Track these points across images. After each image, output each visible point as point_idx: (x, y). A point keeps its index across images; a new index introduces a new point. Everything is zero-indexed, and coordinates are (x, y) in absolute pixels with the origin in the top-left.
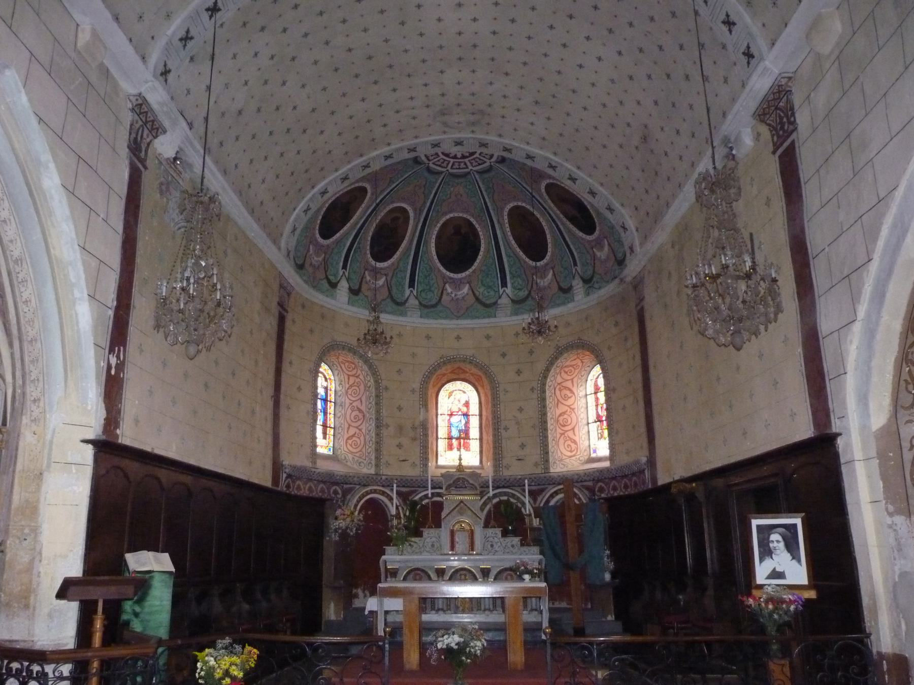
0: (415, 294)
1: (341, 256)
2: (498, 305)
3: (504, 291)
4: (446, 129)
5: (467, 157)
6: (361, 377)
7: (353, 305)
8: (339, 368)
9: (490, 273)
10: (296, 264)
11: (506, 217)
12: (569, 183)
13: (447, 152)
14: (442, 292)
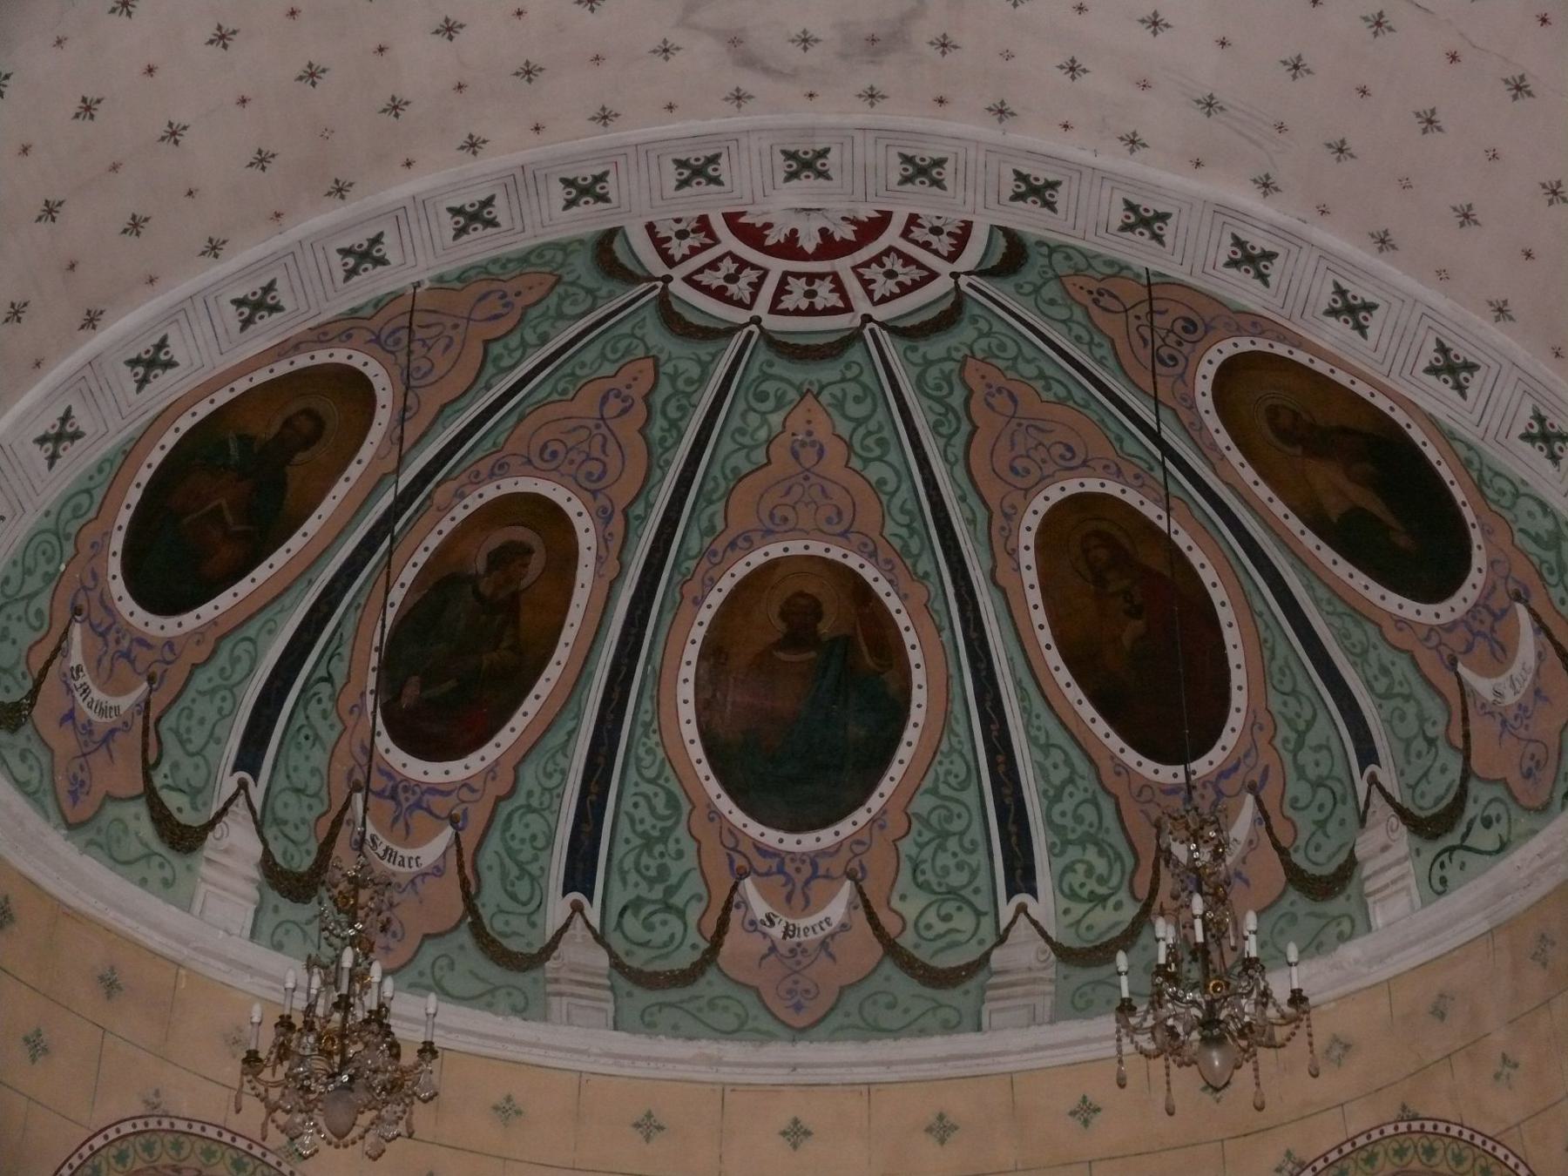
0: (595, 922)
1: (236, 705)
2: (992, 974)
3: (1022, 909)
4: (748, 81)
5: (846, 248)
7: (278, 947)
9: (957, 826)
11: (1028, 558)
12: (1334, 334)
13: (753, 218)
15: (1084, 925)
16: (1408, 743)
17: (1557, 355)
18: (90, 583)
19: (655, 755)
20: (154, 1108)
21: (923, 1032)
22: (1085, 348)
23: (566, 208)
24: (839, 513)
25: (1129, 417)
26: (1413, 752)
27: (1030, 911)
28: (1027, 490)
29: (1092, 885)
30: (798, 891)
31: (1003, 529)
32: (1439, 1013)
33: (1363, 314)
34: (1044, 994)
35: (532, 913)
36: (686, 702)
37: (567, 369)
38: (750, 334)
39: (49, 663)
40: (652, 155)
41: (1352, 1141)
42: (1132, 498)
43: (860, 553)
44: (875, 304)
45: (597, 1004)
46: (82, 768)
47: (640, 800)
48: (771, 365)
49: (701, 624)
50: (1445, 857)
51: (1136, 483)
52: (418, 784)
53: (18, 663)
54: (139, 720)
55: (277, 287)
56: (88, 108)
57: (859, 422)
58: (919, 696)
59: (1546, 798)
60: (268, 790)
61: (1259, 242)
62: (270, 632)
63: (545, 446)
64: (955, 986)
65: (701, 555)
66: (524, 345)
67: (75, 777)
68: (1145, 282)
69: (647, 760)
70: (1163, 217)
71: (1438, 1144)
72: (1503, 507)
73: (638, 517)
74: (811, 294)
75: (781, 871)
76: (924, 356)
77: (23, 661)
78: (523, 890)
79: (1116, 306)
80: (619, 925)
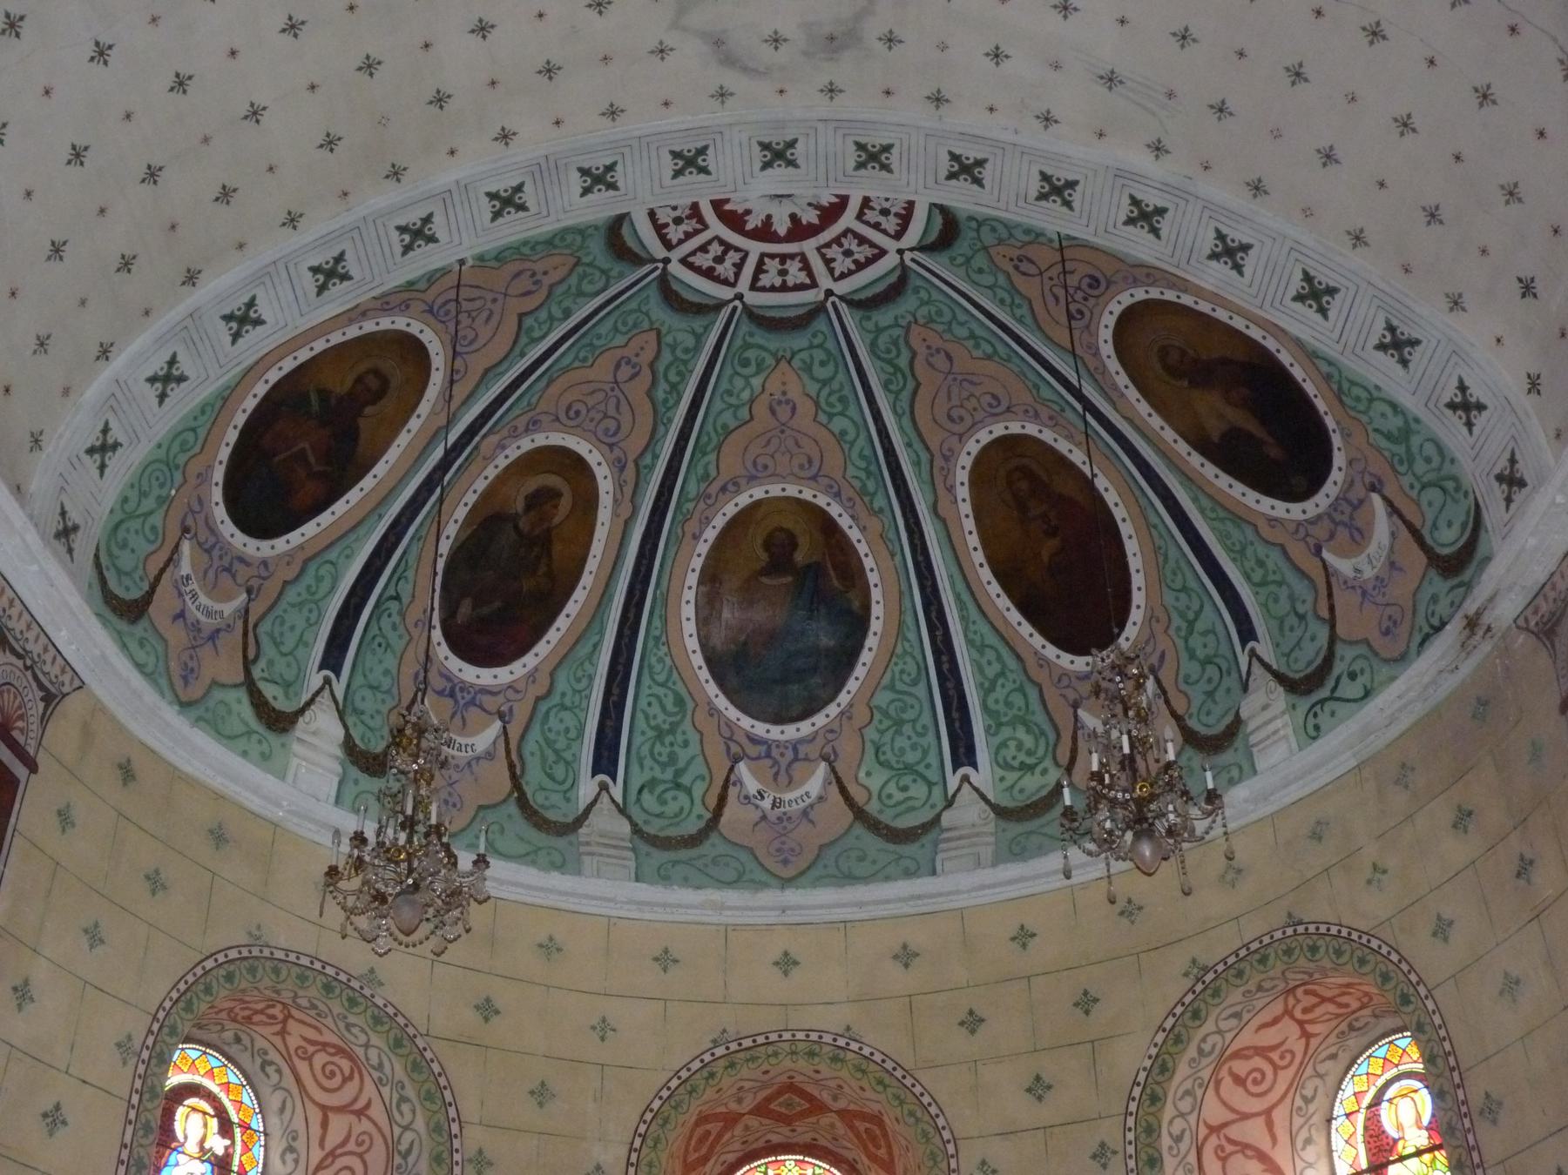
0: (619, 799)
1: (320, 616)
2: (943, 831)
3: (965, 779)
4: (731, 79)
5: (812, 231)
6: (377, 1112)
8: (288, 1080)
10: (109, 598)
11: (963, 492)
12: (1215, 276)
14: (725, 787)
15: (1017, 788)
16: (1282, 621)
17: (1407, 270)
18: (197, 508)
19: (664, 662)
20: (256, 939)
21: (887, 879)
22: (1008, 309)
23: (582, 195)
24: (810, 462)
25: (1043, 367)
26: (1286, 628)
27: (972, 780)
28: (961, 436)
29: (1022, 757)
30: (783, 772)
31: (943, 468)
32: (1316, 836)
33: (1240, 254)
34: (988, 844)
35: (568, 790)
36: (688, 619)
37: (585, 341)
38: (735, 309)
39: (162, 571)
40: (653, 147)
41: (1247, 946)
42: (1047, 436)
43: (826, 493)
44: (836, 280)
45: (621, 862)
46: (191, 658)
47: (652, 699)
48: (751, 335)
49: (699, 555)
50: (1317, 709)
51: (1051, 423)
52: (472, 685)
53: (136, 567)
54: (240, 624)
55: (346, 257)
56: (180, 83)
57: (825, 383)
58: (877, 610)
59: (1403, 648)
60: (348, 686)
61: (1152, 199)
62: (348, 557)
63: (569, 408)
64: (913, 841)
65: (698, 498)
66: (551, 318)
67: (186, 664)
68: (1057, 245)
69: (658, 668)
70: (1072, 185)
71: (1320, 943)
72: (1360, 412)
73: (645, 467)
74: (783, 273)
75: (768, 755)
76: (876, 325)
77: (141, 566)
78: (559, 771)
79: (1033, 270)
80: (638, 800)
